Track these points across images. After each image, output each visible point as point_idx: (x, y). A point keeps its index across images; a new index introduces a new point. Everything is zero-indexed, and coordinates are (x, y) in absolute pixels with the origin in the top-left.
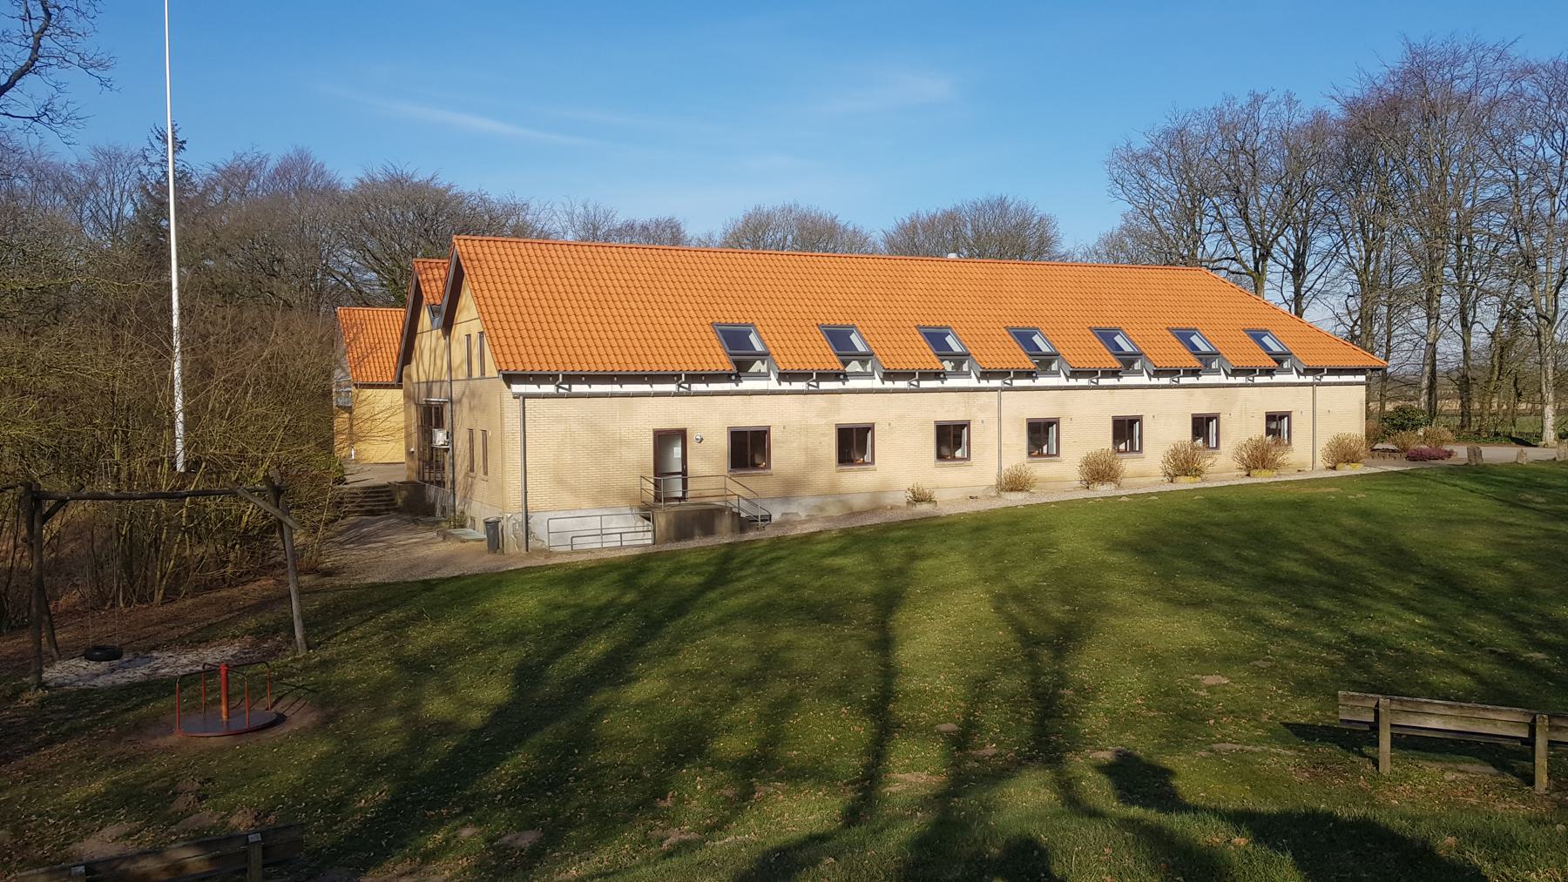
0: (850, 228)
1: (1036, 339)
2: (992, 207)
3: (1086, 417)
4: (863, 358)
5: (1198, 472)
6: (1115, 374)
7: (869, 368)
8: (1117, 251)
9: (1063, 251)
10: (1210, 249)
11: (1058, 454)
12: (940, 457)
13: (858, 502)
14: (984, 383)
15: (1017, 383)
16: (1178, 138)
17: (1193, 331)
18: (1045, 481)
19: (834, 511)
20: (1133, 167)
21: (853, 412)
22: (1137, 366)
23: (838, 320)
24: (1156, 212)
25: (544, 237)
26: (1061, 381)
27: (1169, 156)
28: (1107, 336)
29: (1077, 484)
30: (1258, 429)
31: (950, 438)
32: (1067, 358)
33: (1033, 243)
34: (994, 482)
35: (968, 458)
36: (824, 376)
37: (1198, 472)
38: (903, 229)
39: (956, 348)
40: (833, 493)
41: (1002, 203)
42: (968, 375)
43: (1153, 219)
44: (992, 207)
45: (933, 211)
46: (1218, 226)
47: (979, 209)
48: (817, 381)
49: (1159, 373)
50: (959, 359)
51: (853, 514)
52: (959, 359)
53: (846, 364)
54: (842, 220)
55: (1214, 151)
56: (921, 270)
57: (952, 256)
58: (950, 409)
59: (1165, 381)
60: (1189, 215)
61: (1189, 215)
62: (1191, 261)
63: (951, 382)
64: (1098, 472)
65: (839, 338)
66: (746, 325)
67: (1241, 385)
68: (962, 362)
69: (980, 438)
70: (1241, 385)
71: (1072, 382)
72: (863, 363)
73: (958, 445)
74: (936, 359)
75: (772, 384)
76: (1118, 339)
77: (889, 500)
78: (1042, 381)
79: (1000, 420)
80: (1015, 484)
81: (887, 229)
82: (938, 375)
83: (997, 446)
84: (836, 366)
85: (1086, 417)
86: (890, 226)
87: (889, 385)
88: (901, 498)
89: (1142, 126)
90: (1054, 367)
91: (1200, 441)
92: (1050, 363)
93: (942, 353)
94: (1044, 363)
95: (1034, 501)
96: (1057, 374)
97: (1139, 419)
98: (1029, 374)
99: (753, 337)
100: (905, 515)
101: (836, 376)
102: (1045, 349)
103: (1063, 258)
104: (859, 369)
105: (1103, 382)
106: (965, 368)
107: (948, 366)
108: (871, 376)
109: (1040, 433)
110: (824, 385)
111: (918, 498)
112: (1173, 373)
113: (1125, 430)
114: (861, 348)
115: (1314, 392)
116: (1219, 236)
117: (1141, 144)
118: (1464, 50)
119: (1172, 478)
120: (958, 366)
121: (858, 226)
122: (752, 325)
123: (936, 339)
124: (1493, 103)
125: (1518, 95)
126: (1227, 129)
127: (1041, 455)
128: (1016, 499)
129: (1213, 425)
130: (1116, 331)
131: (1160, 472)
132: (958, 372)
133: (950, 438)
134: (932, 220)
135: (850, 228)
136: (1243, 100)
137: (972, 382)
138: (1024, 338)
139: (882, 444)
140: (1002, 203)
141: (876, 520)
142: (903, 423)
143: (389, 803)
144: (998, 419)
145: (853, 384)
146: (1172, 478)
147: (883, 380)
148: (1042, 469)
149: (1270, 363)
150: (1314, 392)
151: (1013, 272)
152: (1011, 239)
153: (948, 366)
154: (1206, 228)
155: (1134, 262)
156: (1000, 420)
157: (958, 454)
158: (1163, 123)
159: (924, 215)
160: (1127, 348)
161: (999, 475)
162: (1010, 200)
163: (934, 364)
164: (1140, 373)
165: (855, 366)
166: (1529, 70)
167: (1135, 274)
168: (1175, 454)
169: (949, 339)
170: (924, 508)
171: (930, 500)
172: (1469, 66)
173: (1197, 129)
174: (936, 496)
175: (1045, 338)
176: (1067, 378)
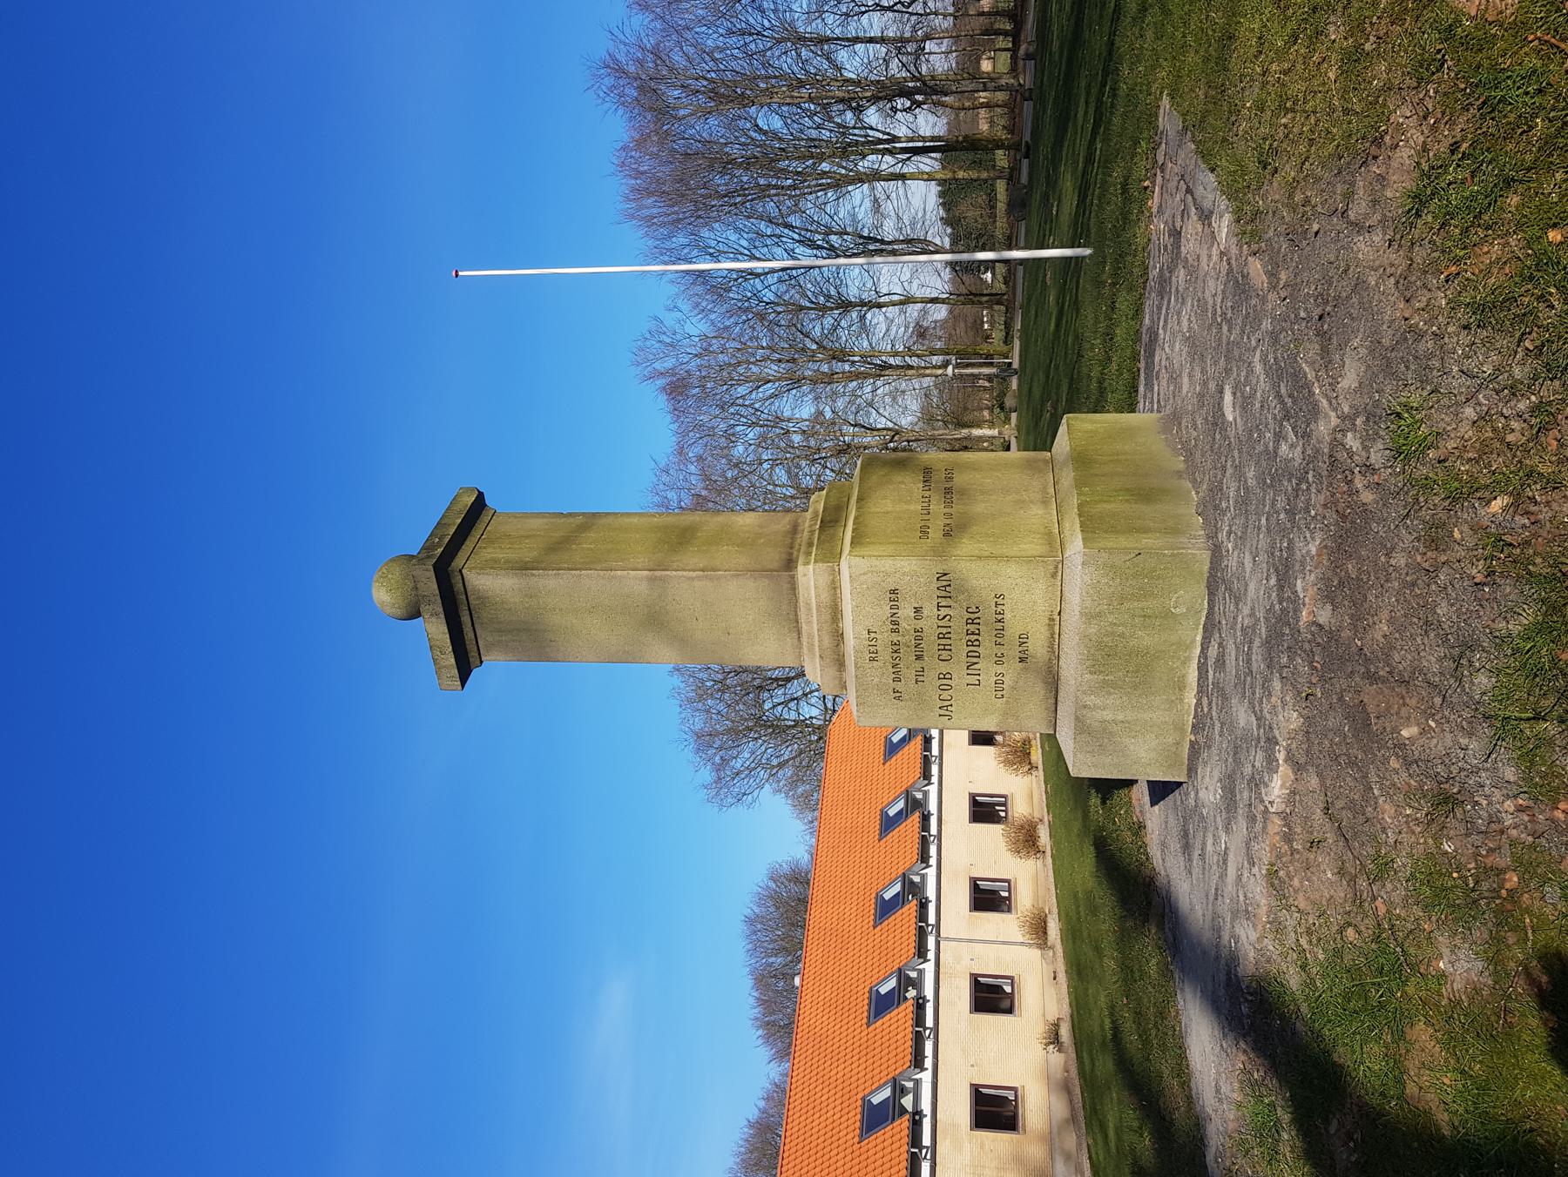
0: (762, 1104)
1: (887, 896)
2: (755, 932)
3: (969, 851)
4: (899, 1091)
5: (1027, 743)
6: (926, 818)
7: (909, 1085)
8: (808, 804)
9: (807, 857)
10: (815, 712)
11: (1008, 881)
12: (1010, 1011)
13: (1060, 1109)
14: (931, 955)
15: (932, 919)
16: (704, 740)
17: (884, 814)
18: (1036, 897)
19: (1070, 1140)
20: (727, 785)
21: (957, 1109)
22: (919, 796)
23: (855, 1118)
24: (775, 762)
25: (779, 1097)
26: (931, 873)
27: (720, 748)
28: (889, 824)
29: (1039, 863)
30: (992, 833)
31: (991, 997)
32: (907, 865)
33: (794, 888)
34: (1039, 952)
35: (1012, 978)
36: (915, 1140)
37: (1027, 743)
38: (767, 1038)
39: (892, 983)
40: (1050, 1139)
41: (750, 921)
42: (921, 972)
43: (781, 765)
44: (755, 932)
45: (752, 1001)
46: (792, 705)
47: (755, 947)
48: (921, 1147)
49: (927, 775)
50: (905, 982)
51: (1073, 1118)
52: (905, 982)
53: (903, 1111)
54: (753, 1114)
55: (721, 707)
56: (811, 1015)
57: (797, 981)
58: (957, 996)
59: (935, 769)
60: (778, 729)
61: (778, 729)
62: (821, 731)
63: (929, 992)
64: (1026, 841)
65: (875, 1118)
66: (863, 1106)
67: (941, 771)
68: (908, 977)
69: (991, 964)
70: (941, 771)
71: (935, 779)
72: (904, 1091)
73: (998, 989)
74: (902, 1007)
75: (926, 1077)
76: (892, 812)
77: (1059, 1074)
78: (931, 893)
79: (971, 941)
80: (1038, 928)
81: (767, 1059)
82: (920, 1006)
83: (999, 944)
84: (904, 1123)
85: (969, 851)
86: (765, 1053)
87: (928, 1063)
88: (1057, 1059)
89: (688, 773)
90: (917, 879)
91: (999, 738)
92: (912, 882)
93: (899, 998)
94: (913, 889)
95: (1055, 910)
96: (923, 877)
97: (975, 978)
98: (923, 906)
100: (1071, 1051)
101: (916, 1124)
102: (897, 888)
103: (814, 856)
104: (910, 1096)
105: (934, 830)
106: (913, 974)
107: (912, 993)
108: (918, 1083)
109: (987, 899)
111: (1054, 1038)
112: (927, 762)
113: (984, 811)
114: (886, 1093)
115: (947, 939)
116: (802, 703)
117: (707, 775)
118: (656, 499)
119: (1033, 767)
121: (761, 1093)
122: (863, 1099)
123: (882, 1005)
124: (706, 478)
125: (700, 458)
126: (702, 694)
127: (1011, 996)
128: (1054, 929)
129: (981, 980)
130: (884, 814)
131: (1027, 779)
132: (917, 984)
133: (991, 997)
134: (761, 1002)
135: (762, 1104)
136: (676, 681)
137: (929, 967)
138: (886, 909)
139: (996, 1076)
140: (750, 921)
141: (1078, 1091)
142: (972, 1052)
144: (971, 944)
145: (926, 1106)
146: (1033, 767)
147: (923, 1069)
148: (1024, 899)
149: (916, 816)
150: (947, 939)
151: (817, 916)
152: (788, 910)
153: (912, 993)
154: (793, 715)
155: (819, 785)
156: (971, 941)
157: (1008, 989)
158: (688, 754)
160: (901, 805)
161: (1030, 945)
163: (907, 1009)
164: (926, 794)
165: (907, 1102)
166: (681, 451)
167: (830, 793)
168: (1008, 763)
169: (883, 990)
170: (1065, 1032)
171: (1056, 1026)
172: (672, 495)
173: (698, 723)
174: (1052, 1018)
176: (928, 866)
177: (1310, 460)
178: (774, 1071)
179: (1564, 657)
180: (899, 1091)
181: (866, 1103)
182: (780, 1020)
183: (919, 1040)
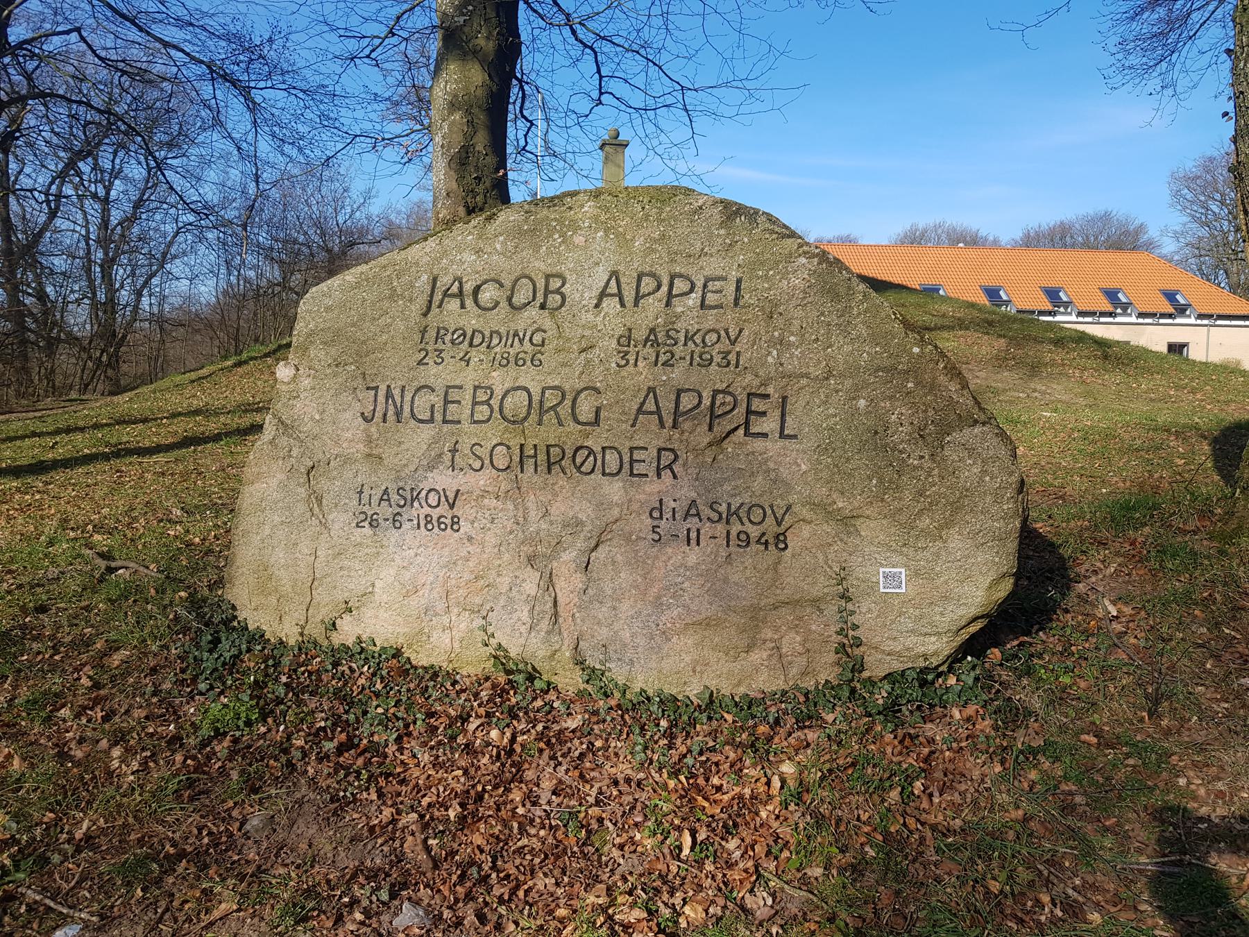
0: (991, 238)
36: (1103, 314)
39: (1124, 300)
42: (1130, 315)
47: (1092, 221)
52: (1067, 305)
54: (983, 233)
63: (1118, 319)
72: (1066, 308)
75: (1133, 319)
78: (1178, 321)
84: (1111, 309)
87: (1141, 320)
98: (1170, 316)
99: (1002, 293)
108: (1070, 314)
110: (1102, 320)
114: (1065, 299)
120: (1125, 309)
123: (1111, 295)
130: (1177, 292)
132: (1125, 313)
143: (1214, 450)
152: (1126, 240)
159: (1045, 227)
162: (1114, 213)
165: (1119, 311)
175: (1066, 293)
177: (292, 745)
178: (1005, 239)
179: (408, 916)
180: (1067, 305)
181: (1177, 292)
182: (1031, 241)
183: (1153, 315)
